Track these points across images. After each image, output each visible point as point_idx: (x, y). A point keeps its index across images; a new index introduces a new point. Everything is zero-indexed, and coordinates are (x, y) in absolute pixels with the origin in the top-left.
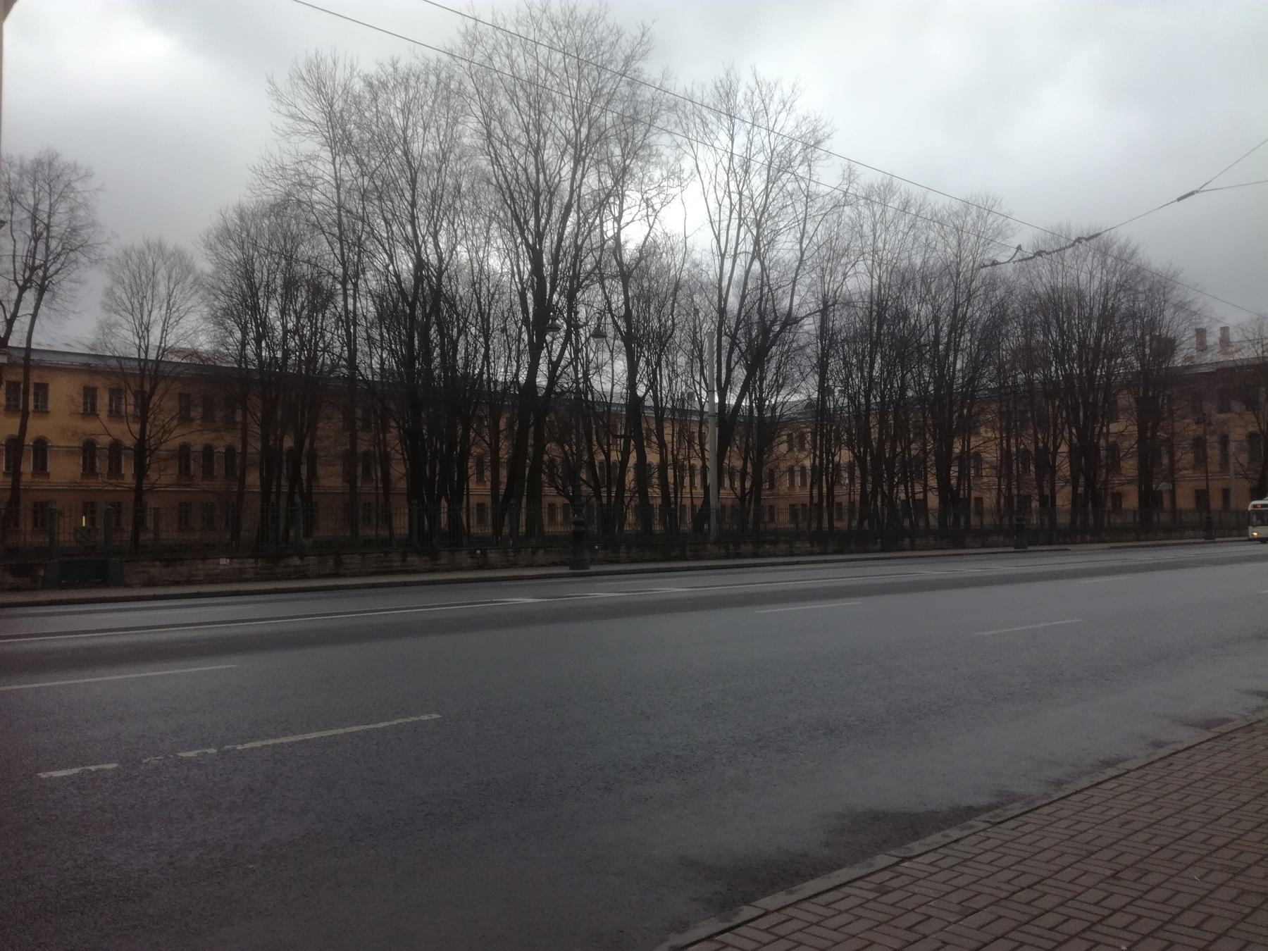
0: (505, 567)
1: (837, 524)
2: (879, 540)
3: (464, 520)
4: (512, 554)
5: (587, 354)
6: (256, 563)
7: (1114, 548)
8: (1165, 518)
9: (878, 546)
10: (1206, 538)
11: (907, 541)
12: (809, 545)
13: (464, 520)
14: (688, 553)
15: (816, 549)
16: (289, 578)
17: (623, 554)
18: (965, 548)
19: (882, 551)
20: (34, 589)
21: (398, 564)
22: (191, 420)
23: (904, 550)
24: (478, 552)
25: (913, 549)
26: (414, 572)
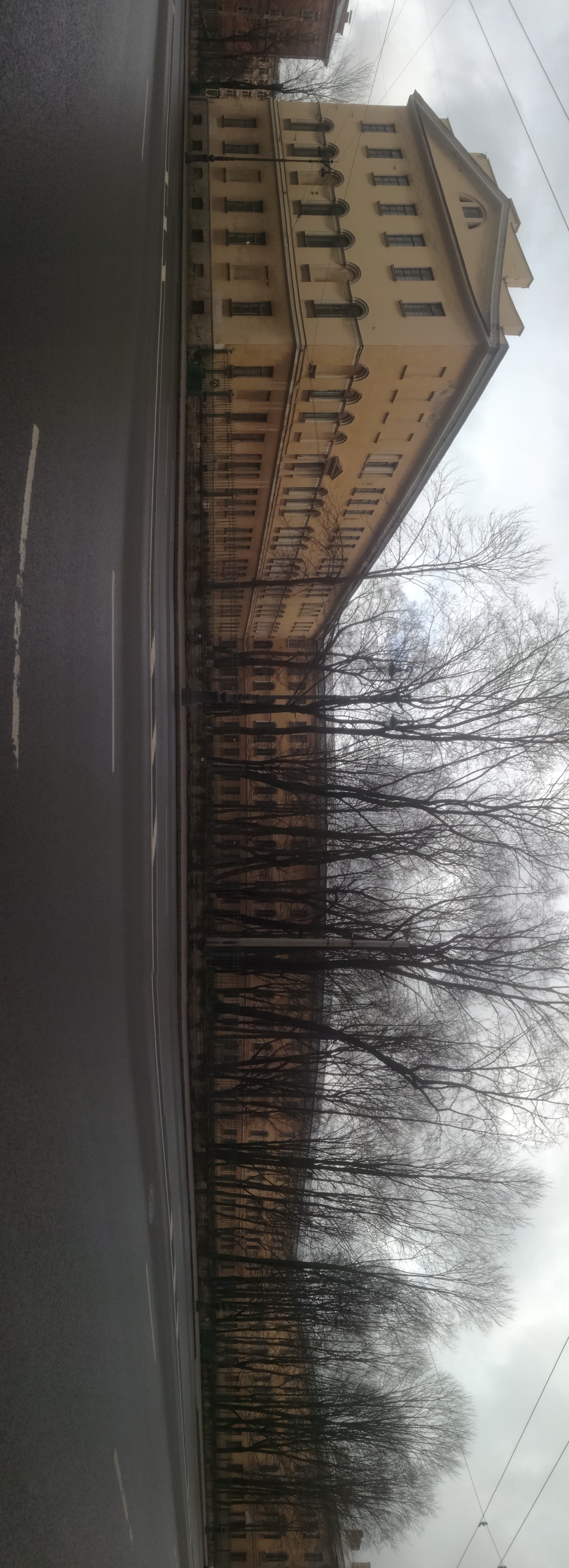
0: (187, 662)
1: (218, 1168)
2: (204, 1150)
3: (267, 974)
4: (198, 671)
5: (461, 910)
6: (197, 463)
7: (197, 1413)
8: (223, 1497)
9: (199, 1150)
10: (207, 1527)
11: (204, 1185)
12: (199, 1053)
13: (267, 974)
14: (195, 873)
15: (196, 1063)
16: (186, 483)
17: (197, 790)
18: (198, 1255)
19: (195, 1154)
20: (187, 360)
21: (192, 564)
22: (226, 506)
23: (195, 1181)
24: (200, 636)
25: (197, 1192)
26: (185, 577)
